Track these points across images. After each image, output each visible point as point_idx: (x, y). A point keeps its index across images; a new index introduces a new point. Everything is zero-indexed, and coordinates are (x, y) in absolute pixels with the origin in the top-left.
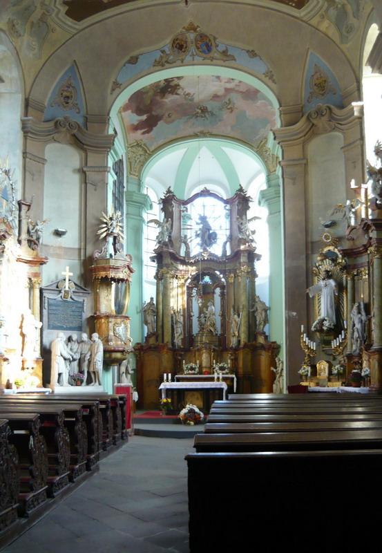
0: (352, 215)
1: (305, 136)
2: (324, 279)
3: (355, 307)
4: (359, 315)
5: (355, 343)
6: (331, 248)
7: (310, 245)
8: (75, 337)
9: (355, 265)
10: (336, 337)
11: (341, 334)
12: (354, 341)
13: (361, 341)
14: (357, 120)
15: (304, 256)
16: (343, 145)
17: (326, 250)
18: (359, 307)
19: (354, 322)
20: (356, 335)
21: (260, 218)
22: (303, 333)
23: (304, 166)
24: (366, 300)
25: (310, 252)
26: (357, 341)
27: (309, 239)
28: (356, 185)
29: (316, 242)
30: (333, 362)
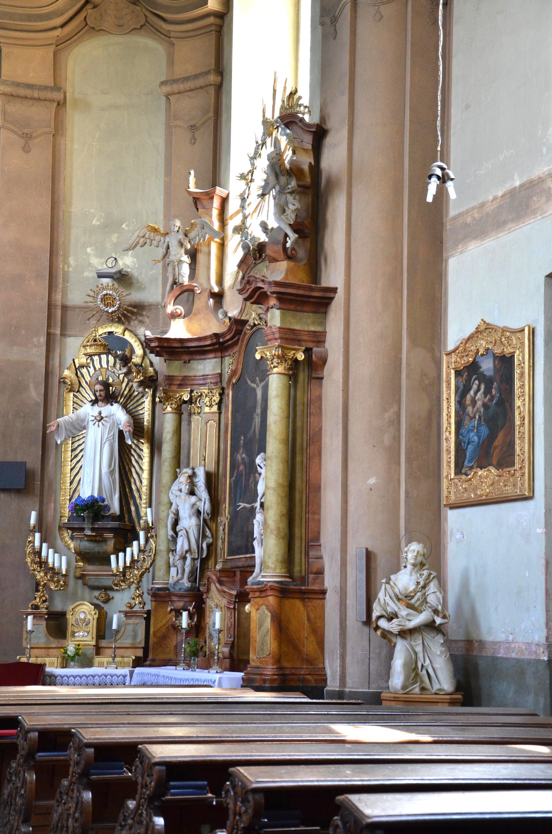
0: (186, 259)
1: (63, 26)
2: (94, 402)
3: (183, 479)
4: (193, 499)
5: (179, 563)
6: (117, 330)
7: (59, 312)
8: (404, 565)
9: (185, 378)
10: (121, 548)
11: (137, 538)
12: (174, 559)
13: (194, 560)
14: (211, 20)
15: (43, 340)
16: (164, 79)
17: (102, 331)
18: (192, 477)
19: (177, 514)
20: (182, 544)
21: (275, 73)
22: (33, 531)
23: (56, 104)
24: (212, 468)
25: (58, 332)
26: (184, 558)
27: (58, 298)
28: (197, 186)
29: (74, 308)
30: (106, 607)
